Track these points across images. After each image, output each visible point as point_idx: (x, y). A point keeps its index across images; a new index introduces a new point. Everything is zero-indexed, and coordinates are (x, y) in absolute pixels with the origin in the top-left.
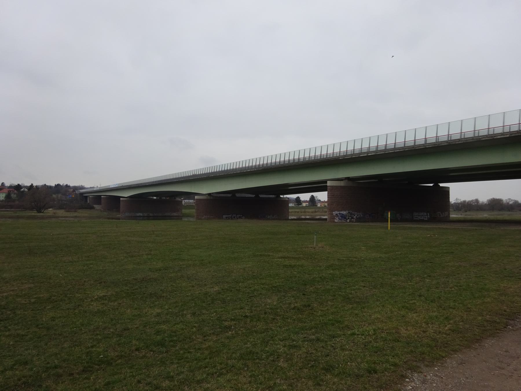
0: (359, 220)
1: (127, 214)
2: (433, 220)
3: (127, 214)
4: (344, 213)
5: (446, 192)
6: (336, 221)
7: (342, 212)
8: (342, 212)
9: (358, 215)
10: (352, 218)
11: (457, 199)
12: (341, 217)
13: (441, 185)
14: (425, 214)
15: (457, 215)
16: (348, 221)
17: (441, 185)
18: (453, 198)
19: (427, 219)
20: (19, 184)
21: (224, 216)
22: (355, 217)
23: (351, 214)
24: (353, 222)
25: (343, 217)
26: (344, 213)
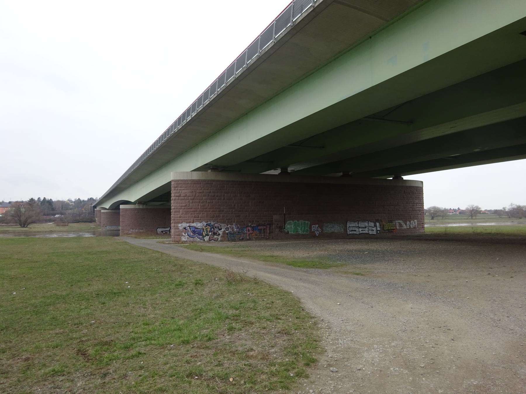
0: (230, 237)
1: (108, 228)
2: (388, 235)
3: (108, 228)
4: (199, 225)
5: (416, 190)
6: (183, 239)
7: (194, 225)
8: (194, 225)
9: (227, 229)
10: (215, 234)
11: (512, 204)
12: (194, 232)
13: (405, 178)
14: (372, 224)
15: (446, 228)
16: (207, 238)
17: (405, 178)
18: (431, 200)
19: (375, 233)
20: (51, 199)
21: (159, 230)
22: (221, 232)
23: (213, 227)
24: (216, 240)
25: (196, 232)
26: (199, 225)
